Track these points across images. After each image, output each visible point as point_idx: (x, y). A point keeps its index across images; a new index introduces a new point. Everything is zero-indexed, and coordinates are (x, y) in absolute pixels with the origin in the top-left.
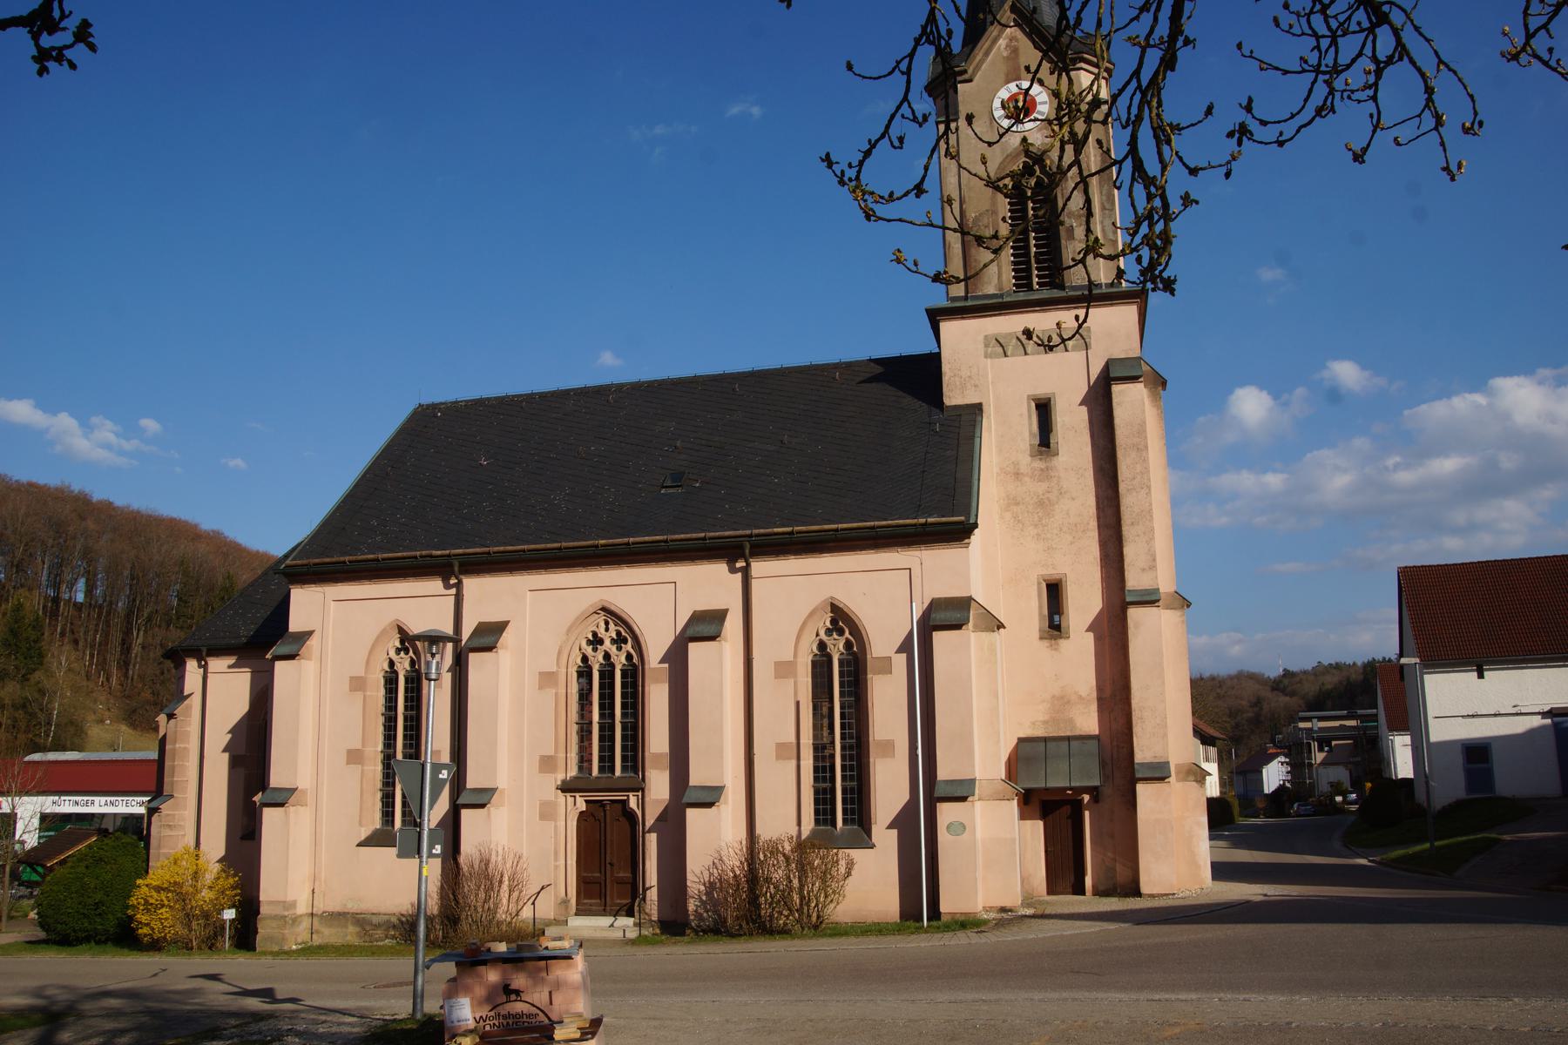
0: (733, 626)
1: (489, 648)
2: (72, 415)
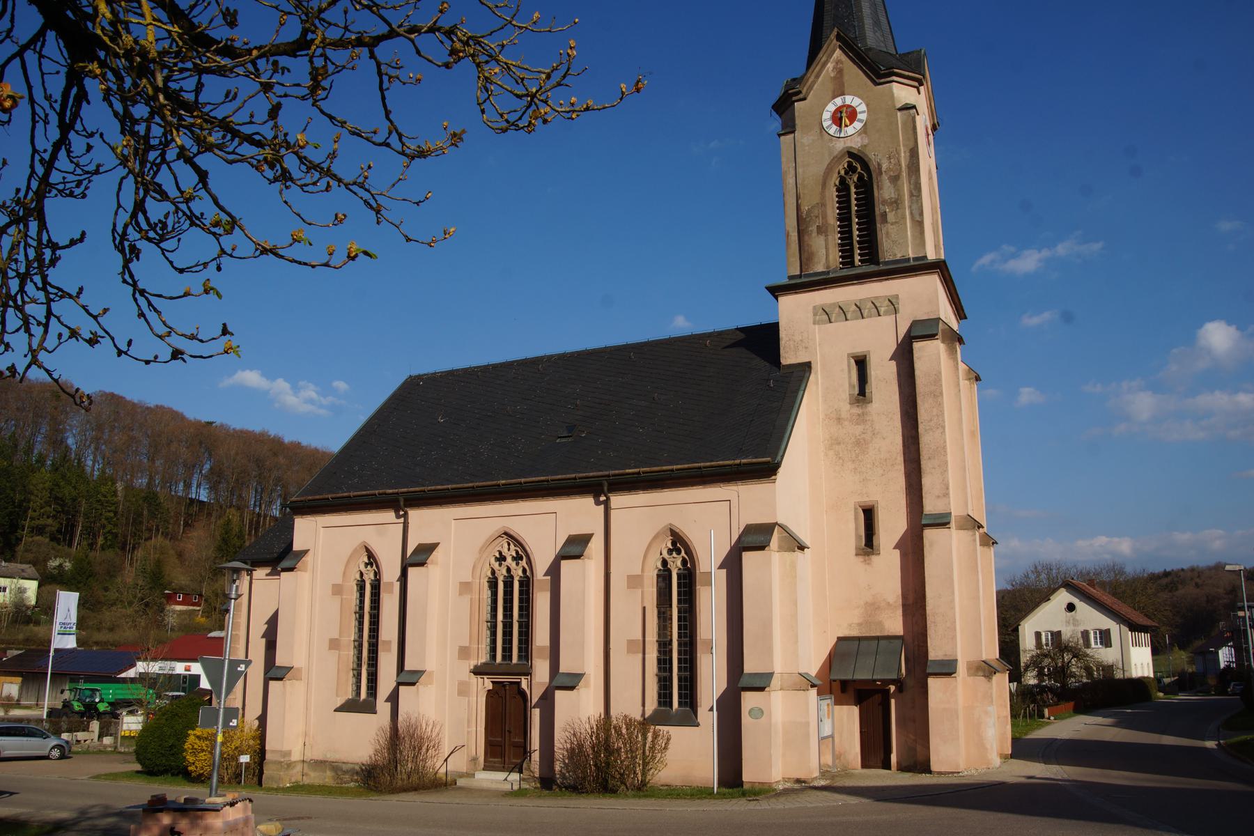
1: (422, 564)
2: (286, 380)
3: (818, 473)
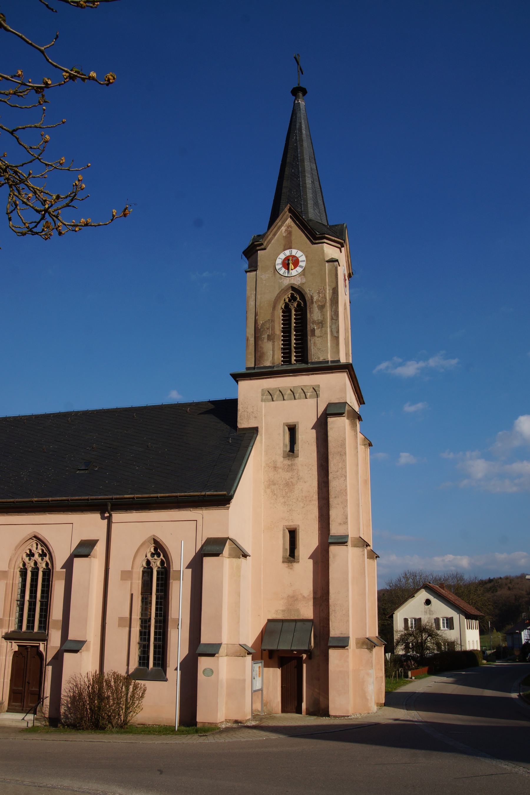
0: (100, 549)
3: (258, 505)
